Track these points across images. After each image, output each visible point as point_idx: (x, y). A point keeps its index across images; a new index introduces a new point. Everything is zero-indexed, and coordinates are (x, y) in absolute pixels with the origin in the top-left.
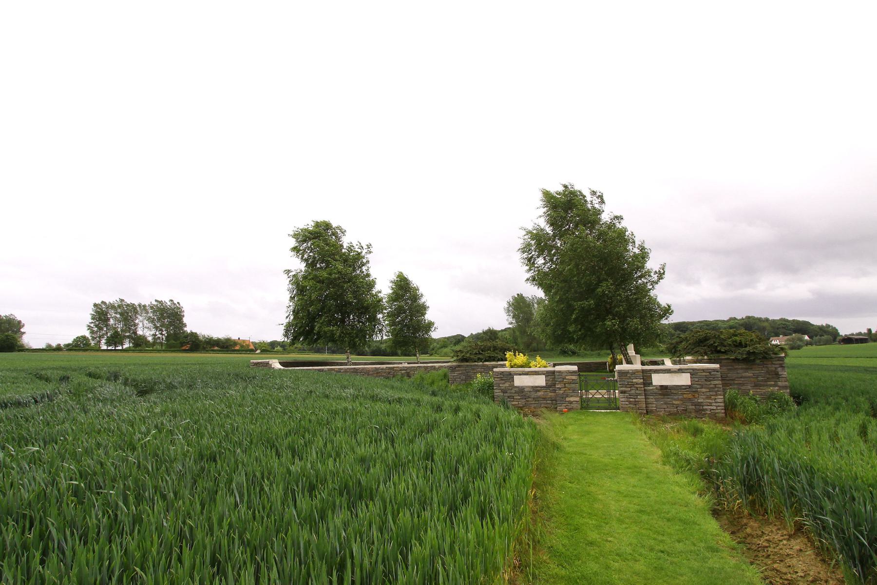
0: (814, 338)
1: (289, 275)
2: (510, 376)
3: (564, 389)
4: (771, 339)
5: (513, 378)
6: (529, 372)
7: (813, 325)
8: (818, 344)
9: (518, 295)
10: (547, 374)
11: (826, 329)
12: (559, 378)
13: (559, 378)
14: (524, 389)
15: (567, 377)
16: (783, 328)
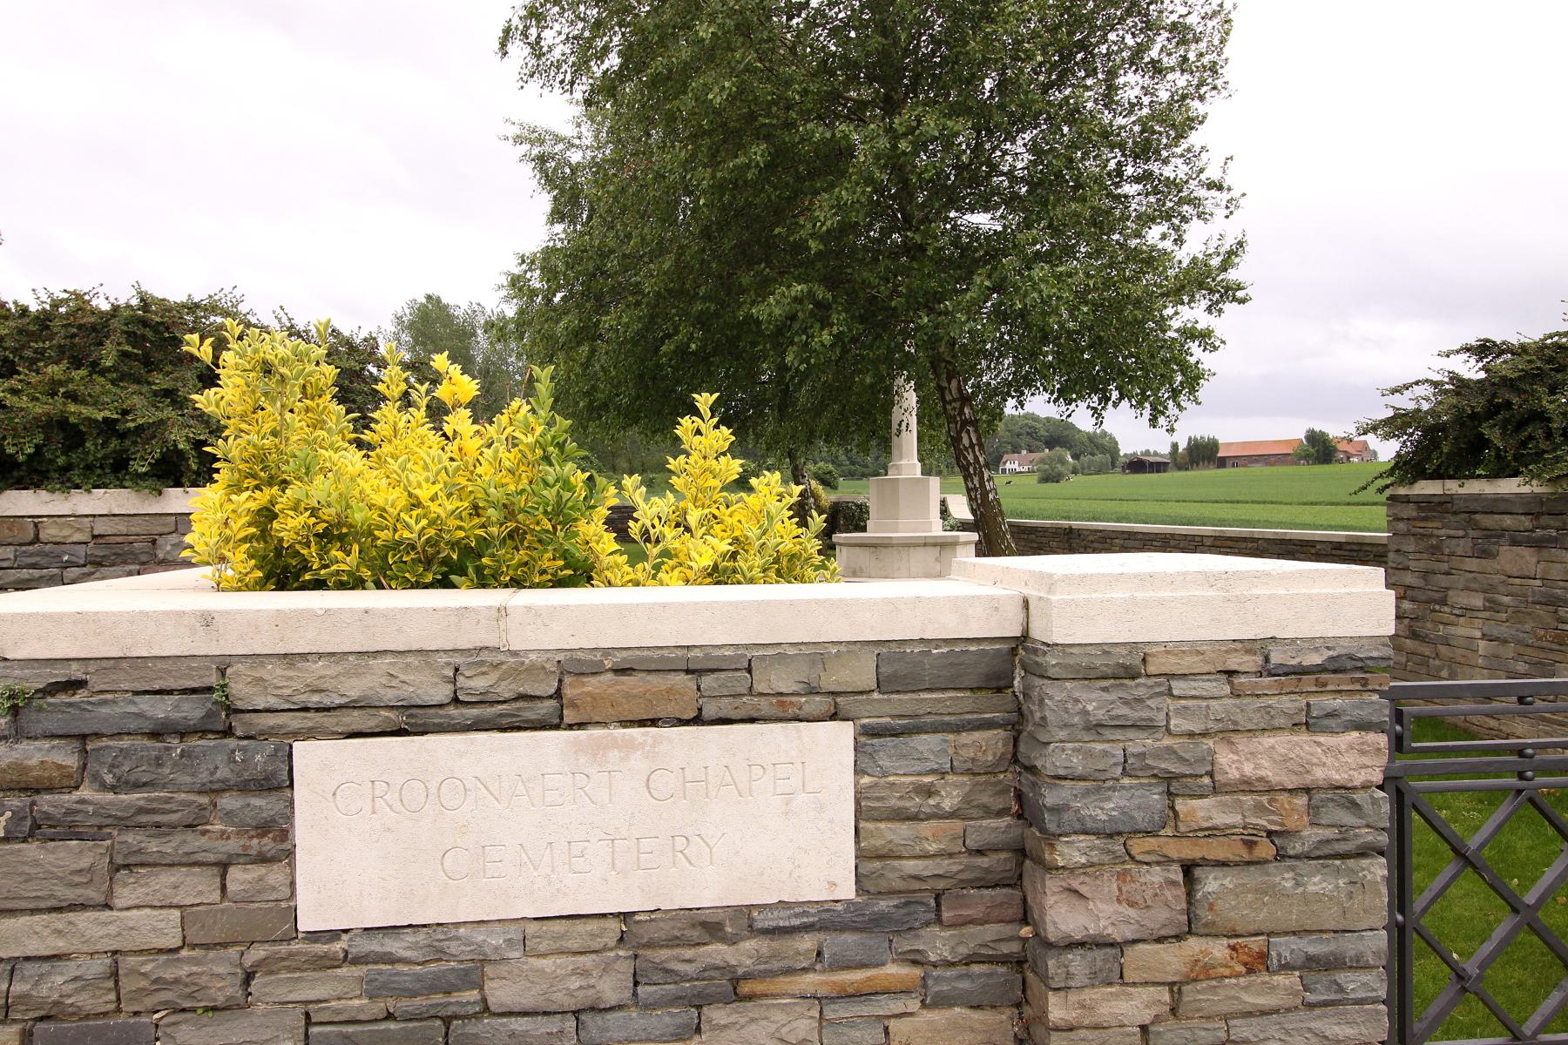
0: (1082, 458)
1: (263, 432)
2: (218, 760)
3: (1173, 959)
4: (1006, 457)
5: (279, 782)
6: (575, 666)
7: (1080, 431)
8: (1086, 471)
9: (429, 297)
10: (884, 708)
11: (1100, 441)
12: (1096, 782)
13: (1096, 782)
14: (474, 972)
15: (1232, 762)
16: (1028, 434)
